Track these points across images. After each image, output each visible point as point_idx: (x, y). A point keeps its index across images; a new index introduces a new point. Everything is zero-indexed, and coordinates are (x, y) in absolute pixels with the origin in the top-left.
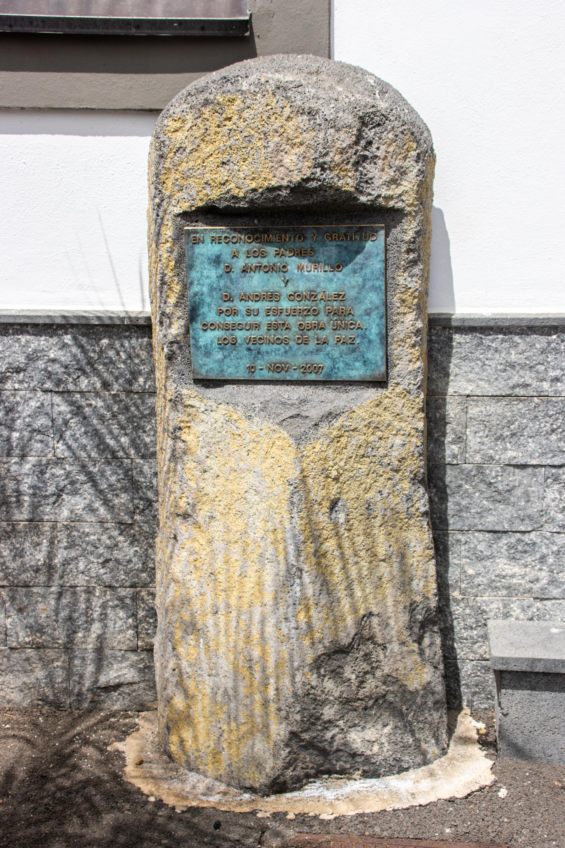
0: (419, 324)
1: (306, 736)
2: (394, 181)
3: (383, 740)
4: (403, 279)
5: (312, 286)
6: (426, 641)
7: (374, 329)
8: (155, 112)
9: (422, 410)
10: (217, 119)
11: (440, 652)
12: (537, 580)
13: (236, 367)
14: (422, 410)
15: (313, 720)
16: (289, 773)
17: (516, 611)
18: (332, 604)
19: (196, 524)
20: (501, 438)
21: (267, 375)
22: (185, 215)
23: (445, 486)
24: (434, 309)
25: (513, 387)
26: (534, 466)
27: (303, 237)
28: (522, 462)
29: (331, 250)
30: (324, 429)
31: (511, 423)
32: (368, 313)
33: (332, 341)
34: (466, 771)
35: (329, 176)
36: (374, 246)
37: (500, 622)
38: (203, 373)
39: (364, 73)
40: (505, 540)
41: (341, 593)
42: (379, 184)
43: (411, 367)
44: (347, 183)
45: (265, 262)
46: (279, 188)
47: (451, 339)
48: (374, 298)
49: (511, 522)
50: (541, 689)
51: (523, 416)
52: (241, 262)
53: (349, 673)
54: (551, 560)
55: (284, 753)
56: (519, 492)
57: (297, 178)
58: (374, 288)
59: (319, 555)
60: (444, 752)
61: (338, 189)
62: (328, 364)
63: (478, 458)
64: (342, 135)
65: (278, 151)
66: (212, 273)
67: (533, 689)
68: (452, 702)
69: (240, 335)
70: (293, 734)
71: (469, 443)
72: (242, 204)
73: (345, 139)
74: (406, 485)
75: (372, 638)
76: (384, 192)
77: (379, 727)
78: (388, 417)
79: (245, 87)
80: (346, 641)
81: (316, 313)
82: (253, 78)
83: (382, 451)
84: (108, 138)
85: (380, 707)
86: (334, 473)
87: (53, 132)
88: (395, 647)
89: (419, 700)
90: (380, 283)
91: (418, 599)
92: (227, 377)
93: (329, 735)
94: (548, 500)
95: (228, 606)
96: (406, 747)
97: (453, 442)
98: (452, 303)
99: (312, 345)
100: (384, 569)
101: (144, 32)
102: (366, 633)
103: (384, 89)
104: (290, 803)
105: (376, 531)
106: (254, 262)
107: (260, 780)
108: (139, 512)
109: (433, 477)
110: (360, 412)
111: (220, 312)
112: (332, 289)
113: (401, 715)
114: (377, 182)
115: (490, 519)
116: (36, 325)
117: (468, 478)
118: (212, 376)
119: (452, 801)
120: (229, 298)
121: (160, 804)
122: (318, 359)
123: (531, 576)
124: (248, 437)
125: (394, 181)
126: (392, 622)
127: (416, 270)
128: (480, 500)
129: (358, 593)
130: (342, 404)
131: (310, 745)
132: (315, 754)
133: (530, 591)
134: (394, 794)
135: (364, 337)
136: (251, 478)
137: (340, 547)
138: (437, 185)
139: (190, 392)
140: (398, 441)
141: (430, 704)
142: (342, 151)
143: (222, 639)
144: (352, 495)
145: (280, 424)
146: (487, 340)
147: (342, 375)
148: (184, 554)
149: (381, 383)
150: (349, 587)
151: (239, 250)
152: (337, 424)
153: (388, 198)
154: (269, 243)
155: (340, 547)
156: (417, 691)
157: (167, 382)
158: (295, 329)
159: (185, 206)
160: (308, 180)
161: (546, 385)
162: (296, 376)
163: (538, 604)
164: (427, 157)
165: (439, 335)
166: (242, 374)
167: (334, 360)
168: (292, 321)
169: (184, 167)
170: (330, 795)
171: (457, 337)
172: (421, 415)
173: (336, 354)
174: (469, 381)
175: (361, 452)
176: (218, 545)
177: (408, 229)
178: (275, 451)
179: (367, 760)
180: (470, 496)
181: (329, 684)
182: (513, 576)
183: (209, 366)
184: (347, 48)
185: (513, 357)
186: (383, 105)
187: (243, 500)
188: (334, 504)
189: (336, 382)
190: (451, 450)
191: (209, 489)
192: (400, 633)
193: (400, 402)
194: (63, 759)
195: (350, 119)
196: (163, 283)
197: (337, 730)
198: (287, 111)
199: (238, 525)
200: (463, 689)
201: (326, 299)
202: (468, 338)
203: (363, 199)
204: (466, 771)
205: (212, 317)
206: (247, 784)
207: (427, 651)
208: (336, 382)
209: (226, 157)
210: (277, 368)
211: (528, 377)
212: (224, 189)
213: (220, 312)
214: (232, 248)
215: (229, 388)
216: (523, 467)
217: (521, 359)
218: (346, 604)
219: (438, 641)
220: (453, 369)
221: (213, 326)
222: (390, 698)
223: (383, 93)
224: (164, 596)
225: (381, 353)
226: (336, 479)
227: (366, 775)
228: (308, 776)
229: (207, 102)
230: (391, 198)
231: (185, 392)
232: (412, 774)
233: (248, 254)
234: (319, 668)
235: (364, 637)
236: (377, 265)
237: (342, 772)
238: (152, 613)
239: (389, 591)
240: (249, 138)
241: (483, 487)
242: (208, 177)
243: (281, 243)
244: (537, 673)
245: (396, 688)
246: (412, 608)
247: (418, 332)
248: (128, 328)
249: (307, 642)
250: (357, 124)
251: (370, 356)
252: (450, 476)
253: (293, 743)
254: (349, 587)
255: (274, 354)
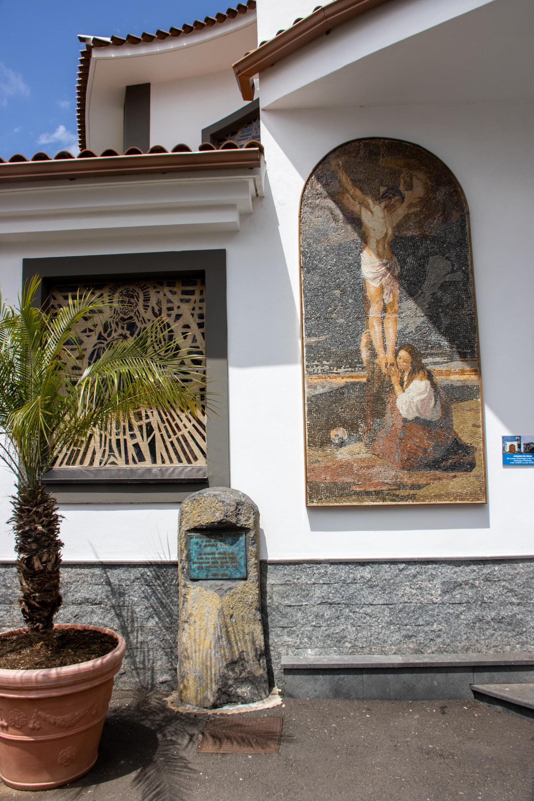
0: (256, 562)
1: (223, 690)
2: (247, 520)
3: (248, 692)
4: (251, 548)
5: (224, 550)
6: (261, 661)
7: (243, 563)
8: (180, 503)
9: (258, 587)
10: (197, 504)
11: (266, 665)
12: (296, 642)
13: (203, 575)
14: (258, 587)
15: (225, 685)
16: (218, 702)
17: (290, 653)
18: (231, 648)
19: (190, 624)
20: (283, 597)
21: (212, 577)
22: (188, 531)
23: (267, 613)
24: (263, 558)
25: (286, 581)
26: (294, 606)
27: (222, 536)
28: (290, 604)
29: (230, 540)
30: (228, 593)
31: (286, 592)
32: (241, 558)
33: (231, 567)
34: (275, 701)
35: (228, 519)
36: (242, 538)
37: (286, 656)
38: (193, 577)
39: (239, 491)
40: (286, 630)
41: (234, 644)
42: (243, 521)
43: (254, 574)
44: (234, 521)
45: (211, 543)
46: (215, 522)
47: (267, 567)
48: (242, 554)
49: (288, 624)
50: (296, 674)
51: (289, 590)
52: (204, 544)
53: (237, 670)
54: (300, 636)
55: (217, 695)
56: (289, 614)
57: (219, 519)
58: (242, 551)
59: (227, 632)
60: (267, 697)
61: (231, 522)
62: (230, 573)
63: (277, 604)
64: (232, 508)
65: (214, 512)
66: (196, 547)
67: (294, 674)
68: (271, 684)
69: (204, 565)
70: (219, 689)
71: (274, 599)
72: (204, 527)
73: (232, 509)
74: (254, 610)
75: (244, 659)
76: (244, 523)
77: (246, 687)
78: (247, 589)
79: (205, 495)
80: (236, 660)
81: (226, 558)
82: (207, 493)
83: (246, 600)
84: (162, 510)
85: (246, 681)
86: (231, 606)
87: (151, 509)
88: (251, 662)
89: (259, 680)
90: (244, 549)
91: (258, 647)
92: (200, 578)
93: (231, 690)
94: (298, 617)
95: (199, 650)
96: (255, 694)
97: (269, 599)
98: (267, 556)
99: (225, 568)
100: (247, 637)
101: (178, 482)
102: (242, 657)
103: (244, 495)
104: (218, 711)
105: (244, 625)
106: (208, 544)
107: (209, 704)
108: (172, 623)
109: (263, 609)
110: (239, 588)
111: (198, 559)
112: (230, 551)
113: (253, 684)
114: (242, 520)
115: (281, 623)
116: (144, 565)
117: (274, 610)
118: (195, 578)
119: (268, 709)
120: (200, 554)
121: (178, 712)
122: (227, 572)
123: (294, 641)
124: (206, 596)
125: (247, 520)
126: (250, 654)
127: (254, 546)
128: (278, 617)
129: (239, 645)
130: (234, 585)
131: (225, 693)
132: (226, 696)
133: (294, 646)
134: (252, 708)
135: (240, 565)
136: (207, 609)
137: (233, 630)
138: (261, 522)
139: (189, 583)
140: (251, 597)
141: (263, 681)
142: (232, 512)
143: (197, 660)
144: (237, 613)
145: (215, 591)
146: (278, 567)
147: (234, 577)
148: (187, 634)
149: (245, 579)
150: (236, 643)
151: (203, 540)
152: (232, 591)
153: (246, 525)
154: (212, 538)
155: (233, 630)
156: (258, 677)
157: (182, 580)
158: (220, 563)
159: (188, 528)
160: (222, 520)
161: (295, 580)
162: (220, 577)
163: (297, 650)
164: (257, 514)
165: (263, 566)
166: (204, 577)
167: (231, 572)
168: (219, 561)
169: (188, 517)
170: (231, 709)
171: (269, 566)
172: (258, 589)
173: (232, 570)
174: (273, 580)
175: (240, 600)
176: (197, 630)
177: (252, 534)
178: (214, 600)
179: (243, 698)
180: (275, 616)
181: (230, 673)
182: (289, 641)
183: (194, 575)
184: (234, 485)
185: (286, 572)
186: (243, 500)
187: (203, 609)
188: (231, 616)
189: (232, 579)
190: (269, 601)
191: (194, 613)
192: (253, 658)
193: (251, 585)
194: (146, 702)
195: (234, 503)
196: (181, 550)
197: (233, 688)
198: (217, 501)
199: (204, 623)
200: (275, 680)
201: (229, 554)
202: (272, 566)
203: (238, 525)
204: (275, 701)
205: (196, 560)
206: (205, 706)
207: (262, 664)
208: (232, 579)
209: (200, 514)
210: (214, 575)
211: (290, 578)
212: (199, 523)
213: (198, 559)
214: (202, 540)
215: (200, 582)
216: (290, 606)
217: (288, 573)
218: (235, 648)
219: (265, 661)
220: (268, 576)
221: (196, 563)
222: (250, 678)
223: (243, 497)
224: (180, 650)
225: (245, 570)
226: (232, 608)
227: (242, 703)
228: (224, 703)
229: (195, 500)
230: (246, 525)
231: (187, 583)
232: (257, 703)
233: (206, 541)
234: (227, 668)
235: (241, 658)
236: (243, 544)
237: (235, 702)
238: (177, 657)
239: (249, 644)
240: (206, 509)
241: (279, 613)
242: (195, 519)
243: (215, 538)
244: (295, 669)
245: (251, 675)
246: (256, 650)
247: (256, 564)
248: (171, 565)
249: (224, 659)
250: (236, 505)
251: (242, 571)
252: (269, 610)
253: (219, 692)
254: (236, 643)
255: (214, 571)
